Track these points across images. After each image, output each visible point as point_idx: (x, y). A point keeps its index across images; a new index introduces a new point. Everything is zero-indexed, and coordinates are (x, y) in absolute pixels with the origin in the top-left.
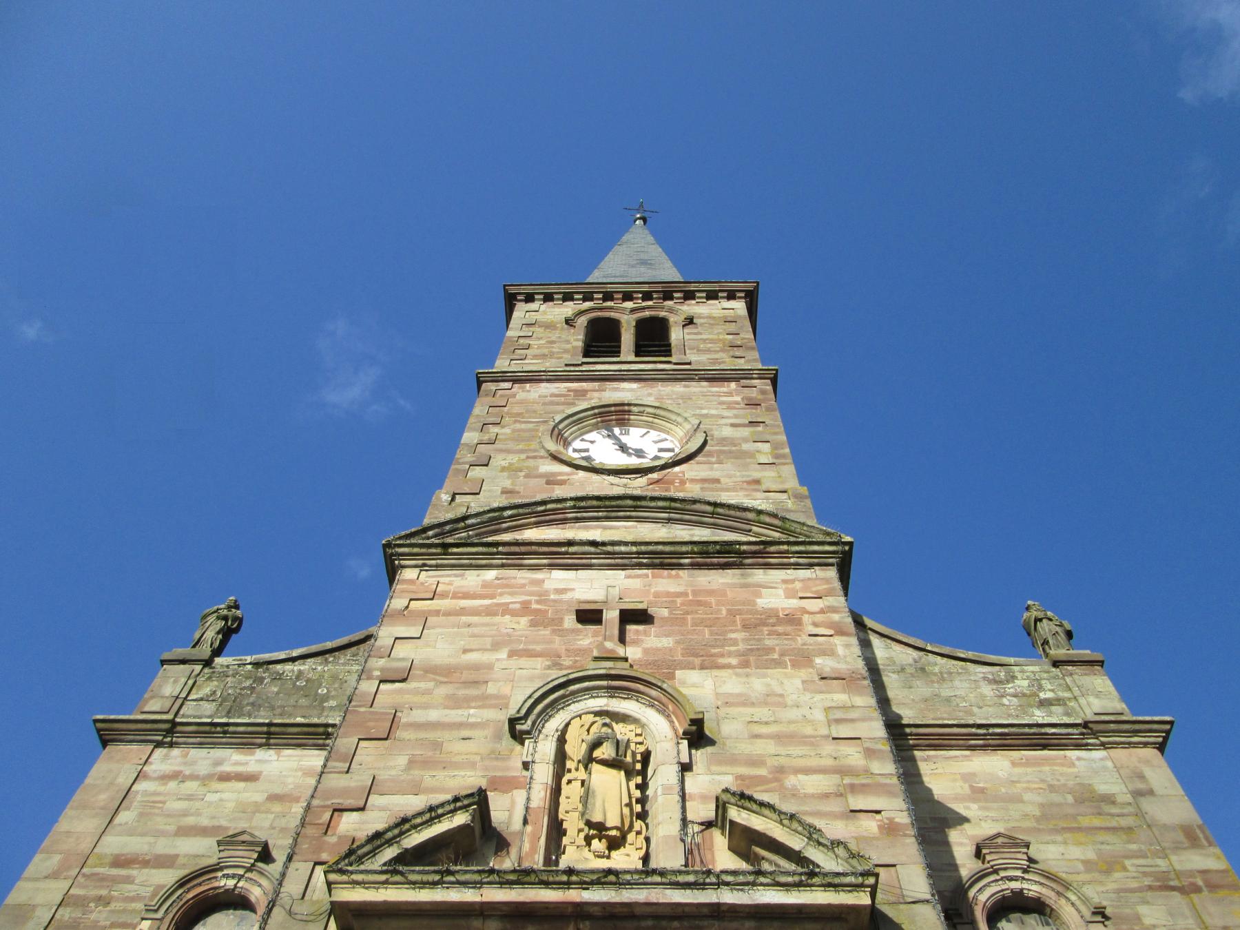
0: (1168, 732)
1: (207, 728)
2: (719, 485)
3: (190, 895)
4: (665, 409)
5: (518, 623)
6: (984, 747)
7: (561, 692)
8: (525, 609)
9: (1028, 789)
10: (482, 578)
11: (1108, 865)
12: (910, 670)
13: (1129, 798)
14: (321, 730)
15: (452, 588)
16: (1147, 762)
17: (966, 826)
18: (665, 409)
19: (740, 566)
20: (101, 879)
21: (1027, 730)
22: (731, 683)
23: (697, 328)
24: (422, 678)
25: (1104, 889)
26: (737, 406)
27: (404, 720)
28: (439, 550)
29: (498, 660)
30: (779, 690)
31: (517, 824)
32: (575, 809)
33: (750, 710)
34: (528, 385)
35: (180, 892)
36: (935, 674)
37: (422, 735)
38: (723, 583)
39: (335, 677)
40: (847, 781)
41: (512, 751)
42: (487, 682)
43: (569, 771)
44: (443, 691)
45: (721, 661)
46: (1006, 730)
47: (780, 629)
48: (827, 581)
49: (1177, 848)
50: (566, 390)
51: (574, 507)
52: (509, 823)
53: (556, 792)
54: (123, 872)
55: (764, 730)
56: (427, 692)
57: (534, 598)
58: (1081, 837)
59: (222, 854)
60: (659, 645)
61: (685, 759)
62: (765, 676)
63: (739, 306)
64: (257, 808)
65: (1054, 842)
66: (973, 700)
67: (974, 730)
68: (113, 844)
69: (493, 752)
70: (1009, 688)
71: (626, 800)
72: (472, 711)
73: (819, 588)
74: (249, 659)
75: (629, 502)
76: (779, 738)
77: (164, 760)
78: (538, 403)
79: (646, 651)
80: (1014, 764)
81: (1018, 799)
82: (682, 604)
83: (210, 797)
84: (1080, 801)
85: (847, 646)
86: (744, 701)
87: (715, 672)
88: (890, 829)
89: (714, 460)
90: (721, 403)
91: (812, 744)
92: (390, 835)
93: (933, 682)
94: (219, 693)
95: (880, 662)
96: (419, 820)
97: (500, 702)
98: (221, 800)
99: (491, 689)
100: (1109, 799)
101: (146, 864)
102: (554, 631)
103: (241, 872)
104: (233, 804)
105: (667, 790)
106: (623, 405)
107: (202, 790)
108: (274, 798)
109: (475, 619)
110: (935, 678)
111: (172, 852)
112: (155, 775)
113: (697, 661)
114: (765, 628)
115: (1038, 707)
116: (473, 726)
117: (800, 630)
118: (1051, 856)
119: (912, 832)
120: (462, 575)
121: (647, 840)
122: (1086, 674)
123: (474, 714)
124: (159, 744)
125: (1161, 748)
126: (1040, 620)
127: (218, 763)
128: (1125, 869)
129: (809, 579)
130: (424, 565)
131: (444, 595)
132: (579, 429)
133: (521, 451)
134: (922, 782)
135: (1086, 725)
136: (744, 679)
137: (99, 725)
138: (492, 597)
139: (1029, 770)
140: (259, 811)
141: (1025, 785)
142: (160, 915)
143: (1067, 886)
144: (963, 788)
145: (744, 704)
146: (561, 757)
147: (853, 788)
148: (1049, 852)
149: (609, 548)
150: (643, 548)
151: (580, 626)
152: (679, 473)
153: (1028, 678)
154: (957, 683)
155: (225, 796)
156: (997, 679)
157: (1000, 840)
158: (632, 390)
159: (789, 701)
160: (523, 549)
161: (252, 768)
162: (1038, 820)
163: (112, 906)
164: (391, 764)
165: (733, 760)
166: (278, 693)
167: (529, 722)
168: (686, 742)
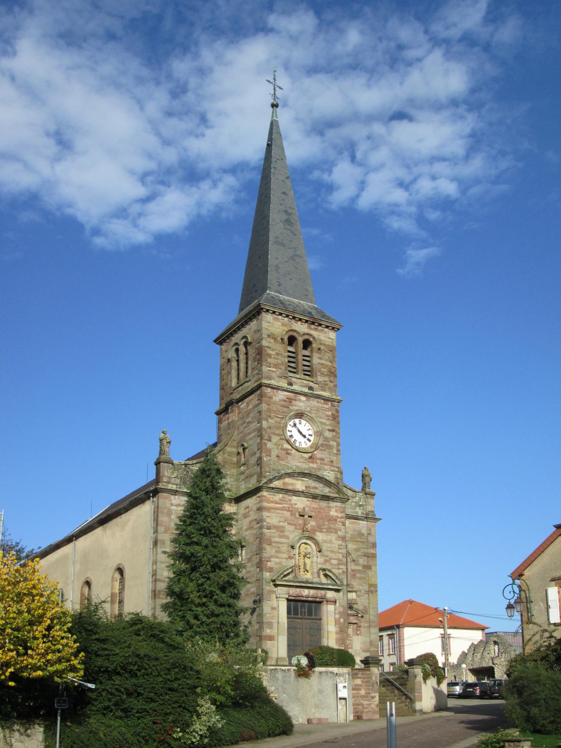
2: (323, 462)
8: (288, 510)
15: (273, 500)
24: (273, 529)
47: (333, 522)
50: (286, 397)
55: (329, 549)
56: (275, 533)
62: (330, 535)
78: (279, 405)
84: (358, 534)
87: (322, 533)
89: (323, 448)
90: (327, 416)
100: (363, 534)
112: (174, 504)
123: (283, 540)
139: (352, 525)
158: (303, 402)
159: (333, 542)
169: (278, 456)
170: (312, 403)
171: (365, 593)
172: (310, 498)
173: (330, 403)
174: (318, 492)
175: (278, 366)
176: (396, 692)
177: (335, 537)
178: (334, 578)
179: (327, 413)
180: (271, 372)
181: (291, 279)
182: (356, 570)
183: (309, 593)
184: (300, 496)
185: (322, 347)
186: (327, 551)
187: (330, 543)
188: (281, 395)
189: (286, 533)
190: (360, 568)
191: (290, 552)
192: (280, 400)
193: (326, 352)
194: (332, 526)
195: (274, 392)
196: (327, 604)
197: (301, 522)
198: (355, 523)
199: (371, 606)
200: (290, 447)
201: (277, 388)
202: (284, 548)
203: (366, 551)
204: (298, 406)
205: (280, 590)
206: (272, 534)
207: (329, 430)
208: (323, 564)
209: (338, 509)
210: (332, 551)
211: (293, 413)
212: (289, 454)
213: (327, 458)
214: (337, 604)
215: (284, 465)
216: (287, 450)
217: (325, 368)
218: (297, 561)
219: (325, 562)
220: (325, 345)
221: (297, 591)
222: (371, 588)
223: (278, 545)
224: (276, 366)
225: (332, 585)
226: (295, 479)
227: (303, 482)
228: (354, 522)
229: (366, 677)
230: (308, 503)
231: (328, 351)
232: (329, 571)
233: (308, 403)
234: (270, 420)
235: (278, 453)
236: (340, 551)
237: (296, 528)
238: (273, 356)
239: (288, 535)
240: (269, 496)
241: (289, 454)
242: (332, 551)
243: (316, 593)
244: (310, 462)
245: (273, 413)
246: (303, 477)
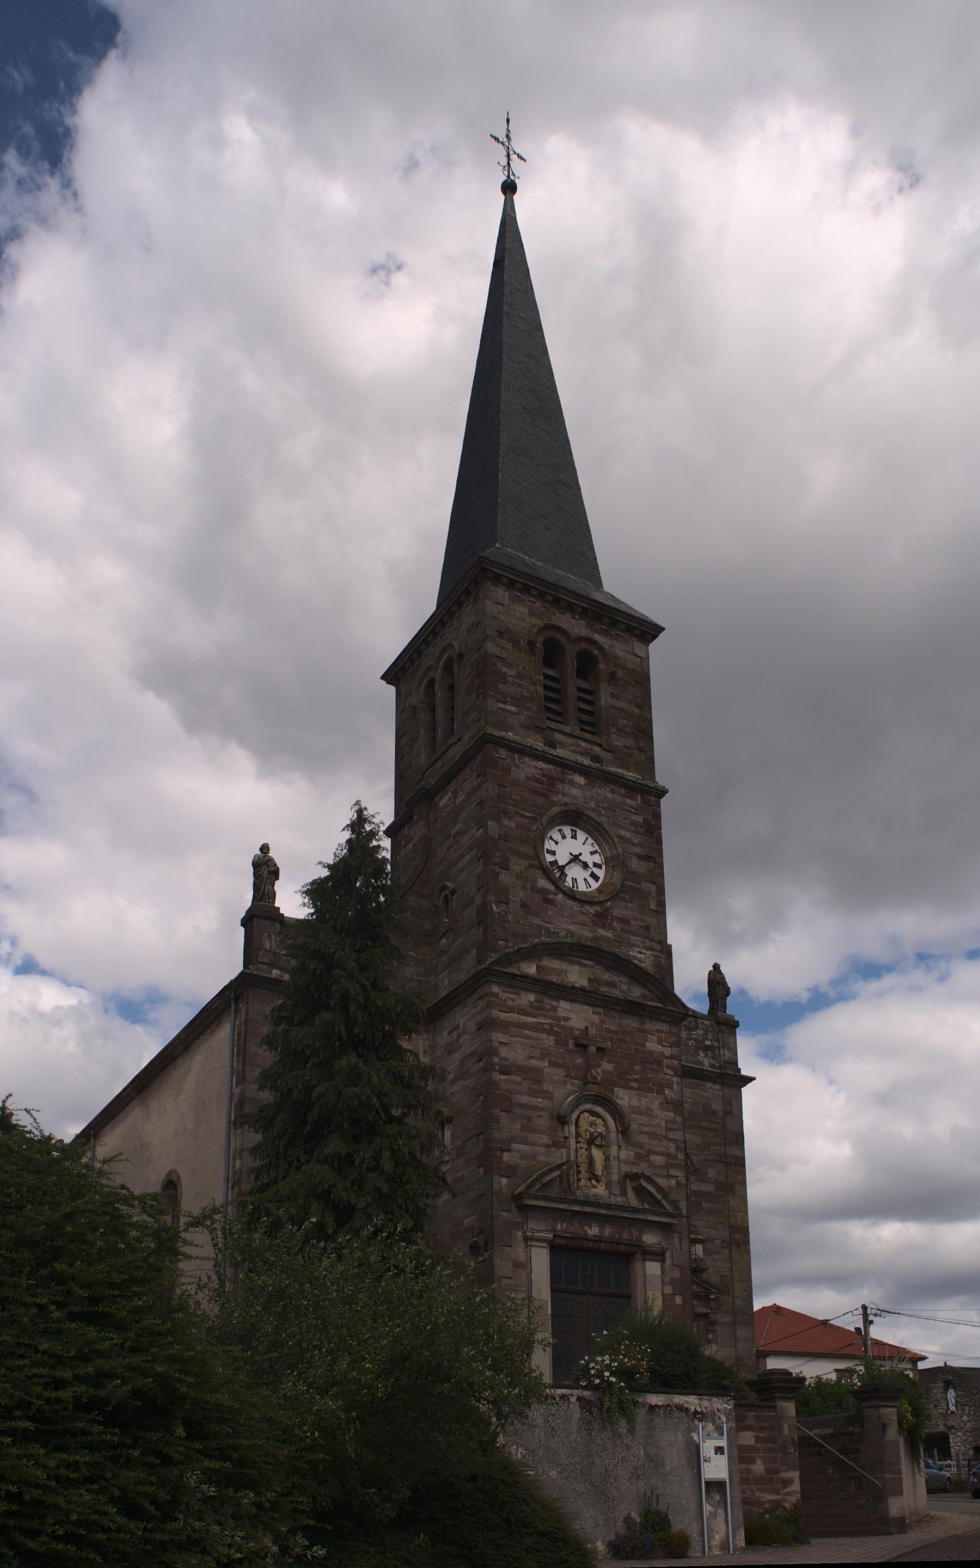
5: (550, 1041)
8: (550, 1032)
25: (699, 1158)
44: (526, 1084)
55: (645, 1129)
56: (519, 1084)
62: (646, 1097)
76: (649, 1134)
90: (633, 823)
100: (714, 1113)
113: (622, 1082)
114: (648, 1065)
116: (542, 1109)
145: (638, 1114)
158: (580, 787)
169: (523, 905)
171: (722, 1247)
174: (616, 993)
176: (830, 1471)
179: (634, 817)
181: (547, 528)
185: (620, 673)
186: (642, 1132)
189: (546, 1086)
190: (710, 1188)
192: (528, 778)
195: (513, 759)
200: (552, 888)
202: (542, 1122)
204: (568, 795)
207: (639, 856)
208: (634, 1163)
210: (652, 1135)
211: (557, 809)
212: (551, 902)
215: (540, 927)
216: (544, 891)
218: (573, 1154)
220: (624, 668)
224: (517, 701)
227: (583, 969)
229: (766, 1425)
231: (632, 682)
232: (648, 1179)
237: (568, 1076)
239: (551, 1089)
242: (652, 1135)
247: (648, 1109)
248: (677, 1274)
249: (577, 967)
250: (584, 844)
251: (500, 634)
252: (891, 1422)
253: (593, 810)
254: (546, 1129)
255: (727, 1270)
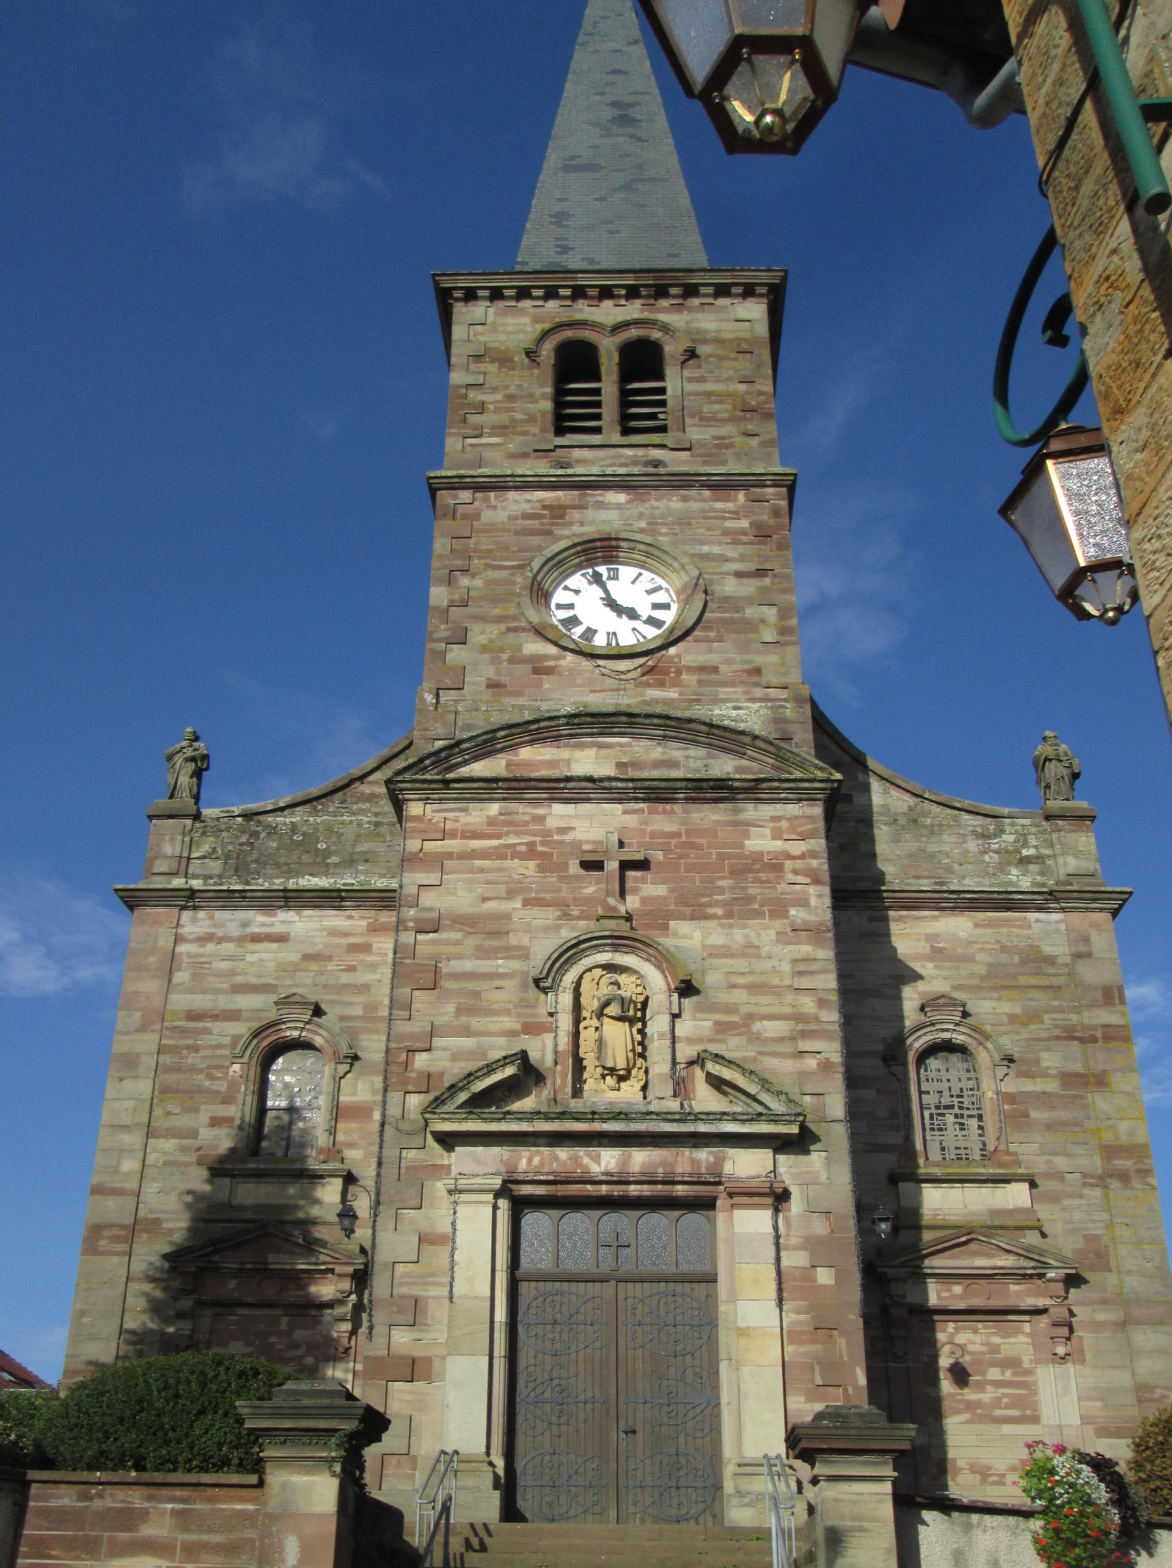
0: (1125, 901)
1: (226, 894)
2: (713, 677)
3: (265, 1044)
4: (659, 548)
5: (527, 868)
6: (952, 909)
7: (574, 951)
8: (531, 853)
9: (982, 950)
10: (484, 813)
11: (1029, 1018)
12: (902, 821)
13: (1068, 959)
14: (335, 894)
15: (458, 826)
16: (1097, 926)
17: (919, 983)
18: (659, 548)
19: (732, 800)
20: (184, 1031)
21: (995, 896)
22: (717, 937)
23: (700, 366)
24: (450, 928)
25: (1016, 1038)
26: (744, 538)
27: (444, 970)
28: (440, 786)
29: (514, 909)
30: (755, 942)
31: (549, 1062)
32: (592, 1051)
33: (729, 961)
34: (492, 494)
35: (255, 1041)
36: (925, 827)
37: (463, 985)
38: (714, 821)
39: (330, 830)
40: (800, 1027)
41: (537, 999)
42: (508, 933)
43: (585, 1019)
44: (471, 942)
45: (710, 911)
46: (976, 896)
47: (763, 876)
48: (811, 819)
49: (1093, 1005)
50: (538, 505)
51: (567, 724)
52: (543, 1062)
53: (576, 1035)
54: (199, 1025)
55: (741, 980)
56: (458, 942)
57: (538, 839)
58: (1015, 994)
59: (281, 1012)
60: (656, 894)
61: (676, 1010)
62: (745, 927)
63: (755, 311)
64: (296, 968)
65: (991, 999)
66: (956, 856)
67: (946, 895)
68: (180, 1001)
69: (522, 1000)
70: (995, 844)
71: (630, 1047)
72: (500, 962)
73: (805, 828)
74: (237, 810)
75: (624, 719)
77: (194, 923)
78: (508, 531)
79: (644, 900)
80: (976, 925)
81: (970, 959)
82: (676, 847)
83: (250, 958)
84: (1024, 962)
85: (820, 896)
86: (726, 952)
87: (704, 923)
88: (825, 1066)
89: (713, 634)
90: (726, 532)
91: (778, 994)
92: (461, 1084)
93: (922, 835)
94: (219, 850)
95: (875, 810)
96: (480, 1074)
97: (523, 953)
98: (261, 960)
99: (513, 940)
100: (1050, 960)
101: (216, 1017)
102: (561, 878)
103: (301, 1025)
104: (273, 964)
105: (661, 1036)
106: (610, 539)
107: (239, 952)
108: (307, 957)
109: (486, 863)
110: (925, 832)
111: (235, 1007)
112: (191, 937)
113: (688, 911)
115: (1016, 866)
117: (781, 877)
118: (983, 1010)
119: (841, 1069)
120: (465, 810)
121: (646, 1072)
122: (1074, 831)
123: (501, 964)
124: (183, 908)
125: (1115, 913)
126: (1050, 760)
127: (246, 924)
128: (1042, 1022)
129: (797, 817)
130: (428, 799)
131: (453, 835)
132: (561, 574)
133: (500, 619)
134: (890, 942)
135: (1051, 893)
136: (726, 931)
137: (121, 893)
138: (498, 836)
139: (989, 931)
140: (298, 970)
141: (980, 946)
142: (245, 1059)
143: (988, 1037)
144: (924, 948)
145: (725, 956)
146: (577, 1006)
147: (804, 1034)
148: (984, 1007)
149: (606, 784)
150: (639, 784)
151: (583, 872)
152: (674, 656)
153: (1016, 832)
154: (945, 837)
155: (264, 956)
156: (986, 833)
157: (941, 1001)
158: (618, 506)
159: (765, 950)
160: (522, 784)
161: (278, 929)
162: (982, 978)
163: (202, 1053)
164: (443, 1011)
165: (713, 1008)
166: (278, 849)
167: (550, 980)
168: (676, 995)
170: (656, 504)
171: (1085, 1185)
172: (637, 800)
173: (741, 496)
175: (511, 429)
177: (772, 934)
178: (752, 1089)
180: (479, 449)
182: (1029, 1094)
183: (625, 1161)
184: (588, 800)
185: (702, 350)
186: (734, 986)
187: (743, 955)
188: (516, 501)
190: (1052, 1086)
191: (534, 1006)
192: (510, 518)
193: (721, 358)
194: (753, 890)
195: (486, 500)
196: (732, 1206)
197: (590, 890)
198: (1007, 921)
199: (1124, 1233)
200: (552, 650)
201: (499, 485)
203: (1074, 1018)
204: (592, 523)
205: (463, 1158)
206: (443, 948)
209: (784, 824)
210: (755, 988)
213: (729, 662)
214: (796, 1205)
217: (722, 402)
219: (717, 1032)
221: (557, 1158)
222: (1116, 1162)
223: (471, 985)
224: (501, 430)
225: (734, 1118)
226: (567, 746)
227: (604, 752)
228: (998, 919)
230: (632, 821)
231: (733, 355)
232: (718, 1058)
233: (644, 508)
234: (465, 581)
235: (498, 673)
236: (805, 982)
238: (491, 407)
239: (525, 941)
240: (438, 817)
241: (549, 671)
243: (663, 1163)
244: (648, 685)
245: (479, 558)
246: (601, 734)
247: (749, 946)
248: (820, 1228)
249: (593, 752)
250: (633, 582)
251: (478, 358)
252: (865, 1524)
253: (642, 531)
254: (511, 1006)
255: (1102, 1225)
